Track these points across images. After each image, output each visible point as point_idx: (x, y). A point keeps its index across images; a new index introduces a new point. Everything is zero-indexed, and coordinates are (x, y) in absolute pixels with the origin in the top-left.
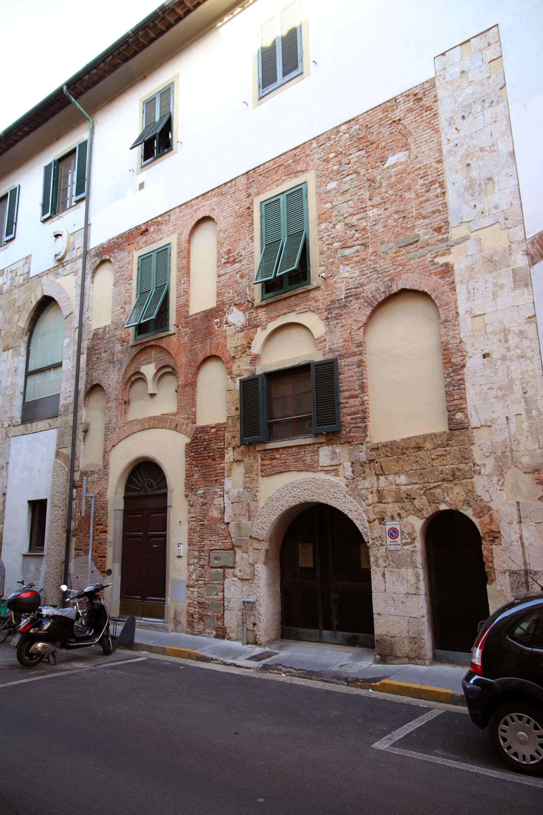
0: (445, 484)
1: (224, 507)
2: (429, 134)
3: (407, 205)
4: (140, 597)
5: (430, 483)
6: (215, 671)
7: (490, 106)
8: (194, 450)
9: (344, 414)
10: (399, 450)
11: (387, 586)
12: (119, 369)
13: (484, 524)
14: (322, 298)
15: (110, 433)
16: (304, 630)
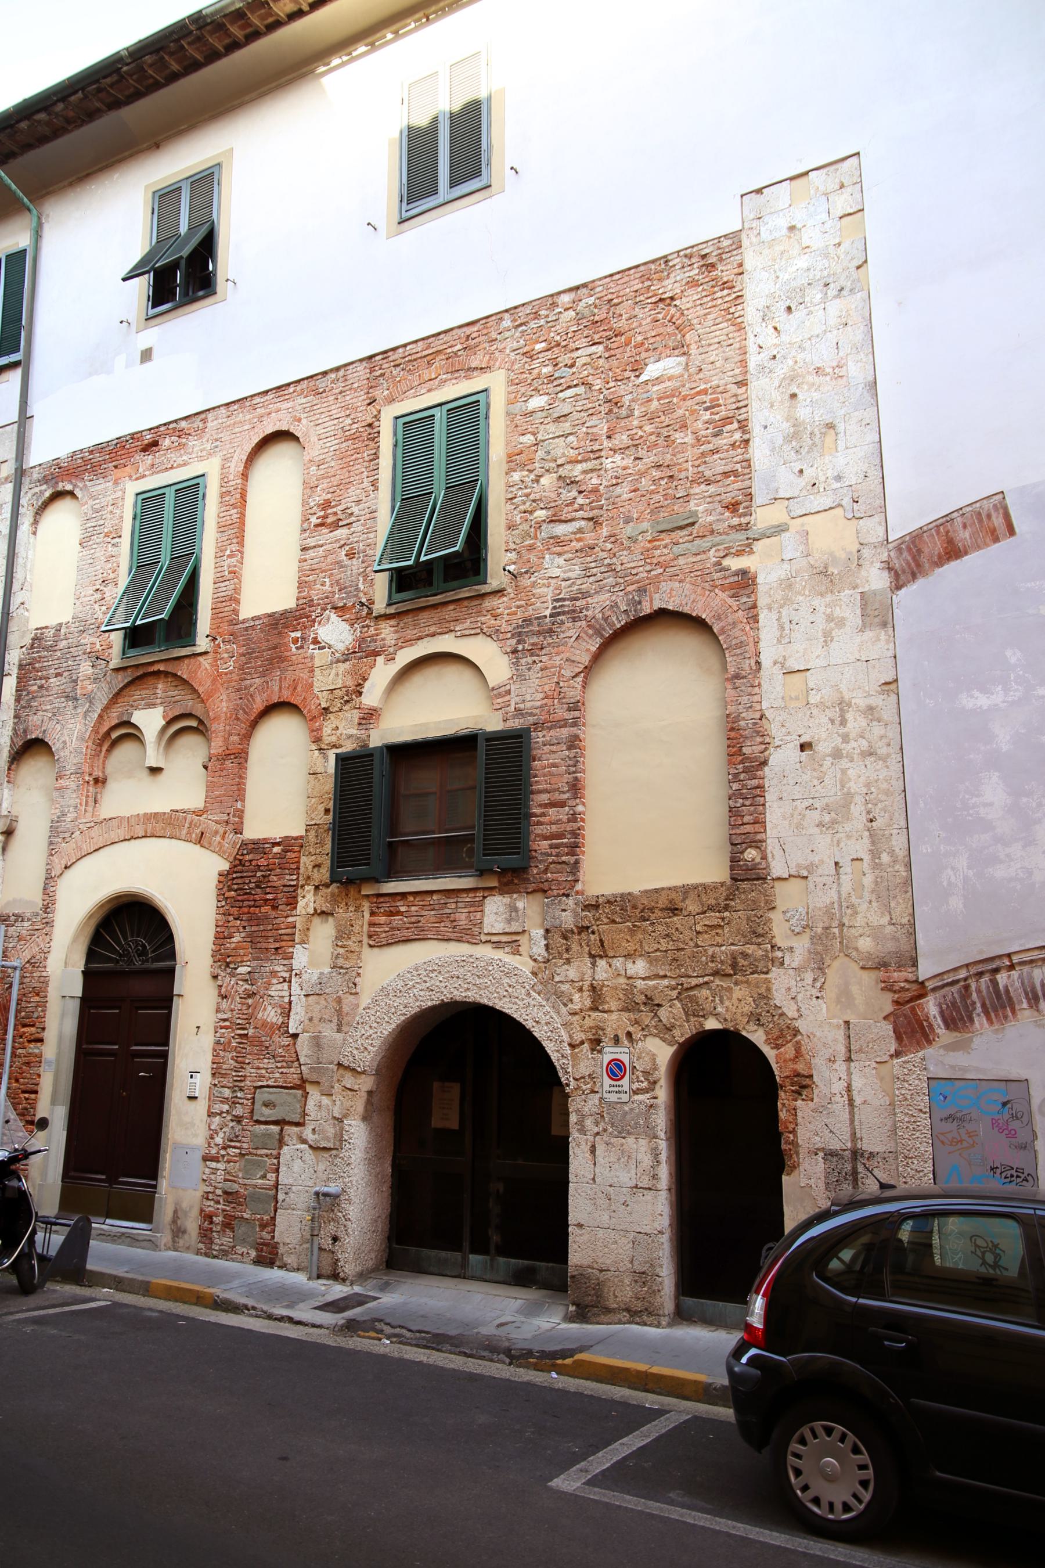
0: (718, 982)
1: (290, 1002)
2: (725, 331)
3: (678, 456)
4: (104, 1177)
5: (691, 977)
6: (250, 1331)
7: (838, 296)
8: (236, 887)
9: (538, 835)
10: (637, 911)
11: (597, 1171)
12: (87, 711)
13: (785, 1061)
14: (507, 611)
15: (60, 840)
16: (433, 1253)
